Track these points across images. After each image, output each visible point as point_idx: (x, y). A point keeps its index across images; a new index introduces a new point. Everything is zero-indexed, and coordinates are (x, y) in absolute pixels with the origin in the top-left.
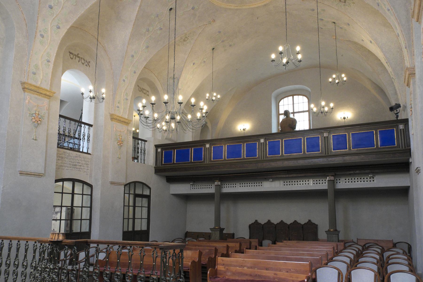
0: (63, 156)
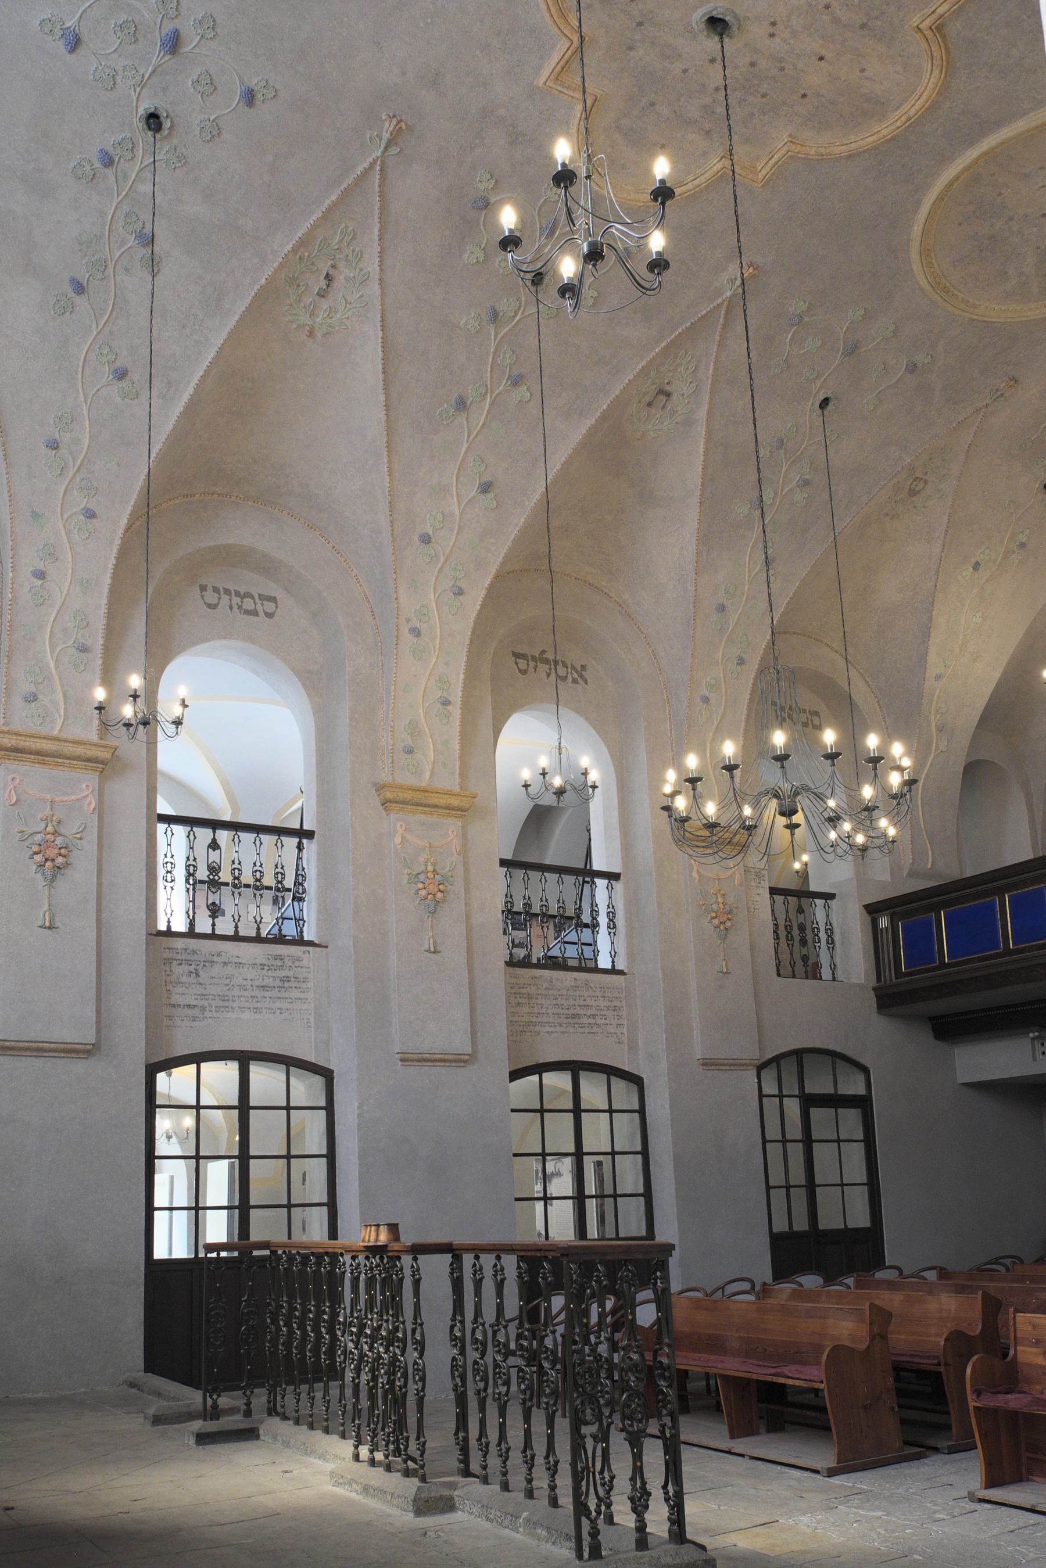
0: (532, 990)
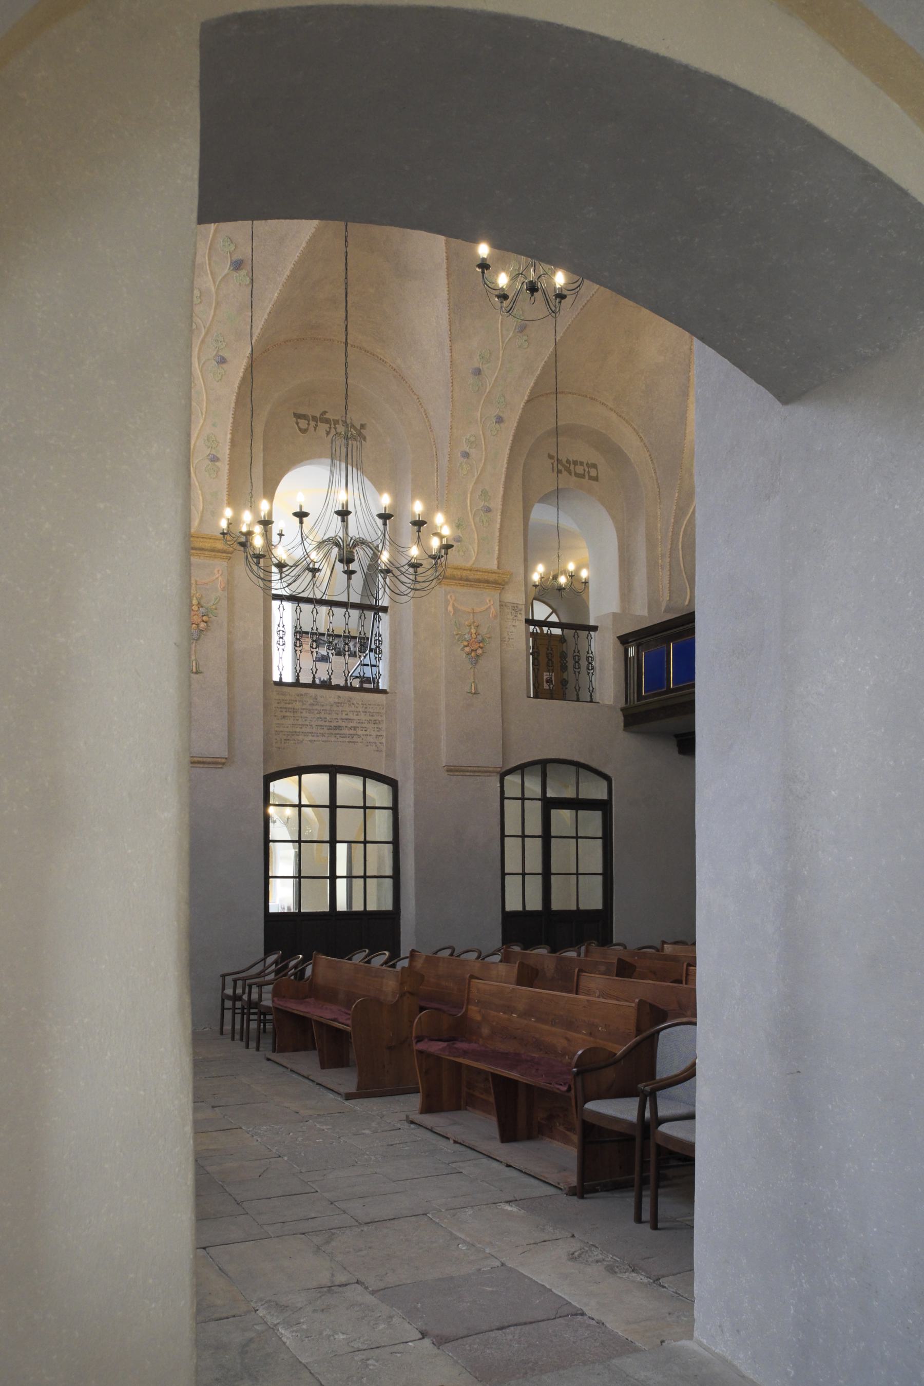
0: (298, 705)
